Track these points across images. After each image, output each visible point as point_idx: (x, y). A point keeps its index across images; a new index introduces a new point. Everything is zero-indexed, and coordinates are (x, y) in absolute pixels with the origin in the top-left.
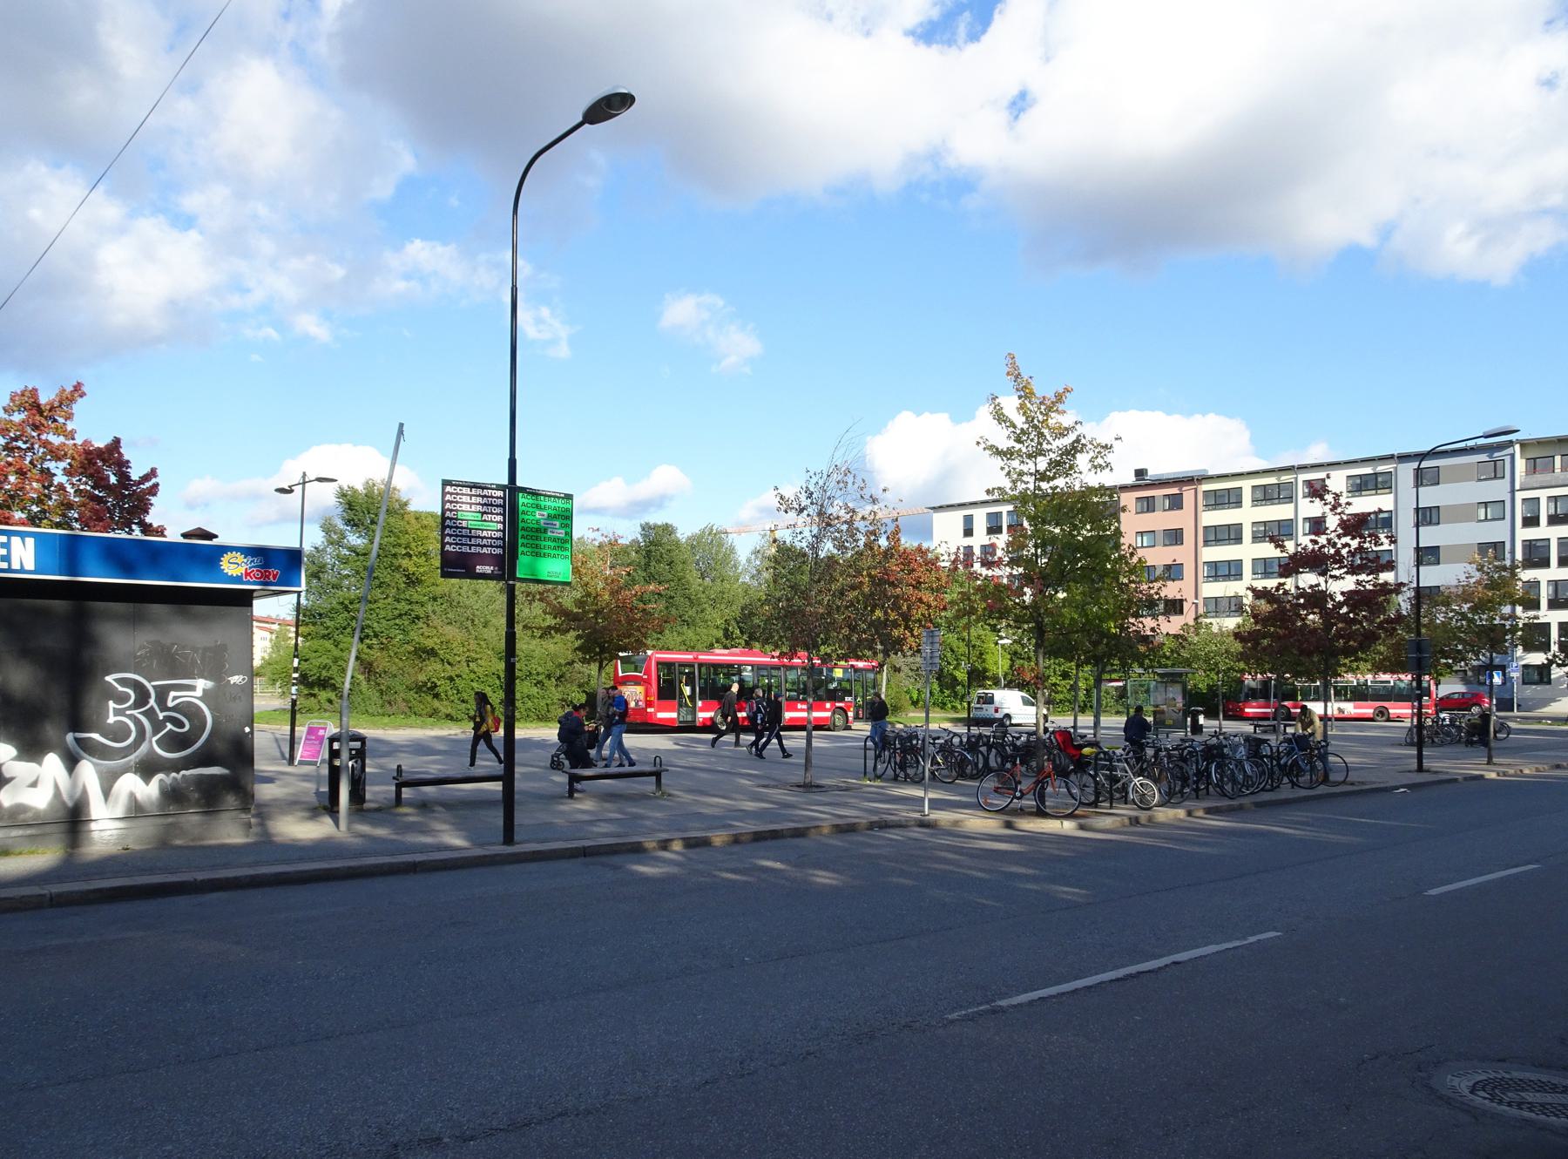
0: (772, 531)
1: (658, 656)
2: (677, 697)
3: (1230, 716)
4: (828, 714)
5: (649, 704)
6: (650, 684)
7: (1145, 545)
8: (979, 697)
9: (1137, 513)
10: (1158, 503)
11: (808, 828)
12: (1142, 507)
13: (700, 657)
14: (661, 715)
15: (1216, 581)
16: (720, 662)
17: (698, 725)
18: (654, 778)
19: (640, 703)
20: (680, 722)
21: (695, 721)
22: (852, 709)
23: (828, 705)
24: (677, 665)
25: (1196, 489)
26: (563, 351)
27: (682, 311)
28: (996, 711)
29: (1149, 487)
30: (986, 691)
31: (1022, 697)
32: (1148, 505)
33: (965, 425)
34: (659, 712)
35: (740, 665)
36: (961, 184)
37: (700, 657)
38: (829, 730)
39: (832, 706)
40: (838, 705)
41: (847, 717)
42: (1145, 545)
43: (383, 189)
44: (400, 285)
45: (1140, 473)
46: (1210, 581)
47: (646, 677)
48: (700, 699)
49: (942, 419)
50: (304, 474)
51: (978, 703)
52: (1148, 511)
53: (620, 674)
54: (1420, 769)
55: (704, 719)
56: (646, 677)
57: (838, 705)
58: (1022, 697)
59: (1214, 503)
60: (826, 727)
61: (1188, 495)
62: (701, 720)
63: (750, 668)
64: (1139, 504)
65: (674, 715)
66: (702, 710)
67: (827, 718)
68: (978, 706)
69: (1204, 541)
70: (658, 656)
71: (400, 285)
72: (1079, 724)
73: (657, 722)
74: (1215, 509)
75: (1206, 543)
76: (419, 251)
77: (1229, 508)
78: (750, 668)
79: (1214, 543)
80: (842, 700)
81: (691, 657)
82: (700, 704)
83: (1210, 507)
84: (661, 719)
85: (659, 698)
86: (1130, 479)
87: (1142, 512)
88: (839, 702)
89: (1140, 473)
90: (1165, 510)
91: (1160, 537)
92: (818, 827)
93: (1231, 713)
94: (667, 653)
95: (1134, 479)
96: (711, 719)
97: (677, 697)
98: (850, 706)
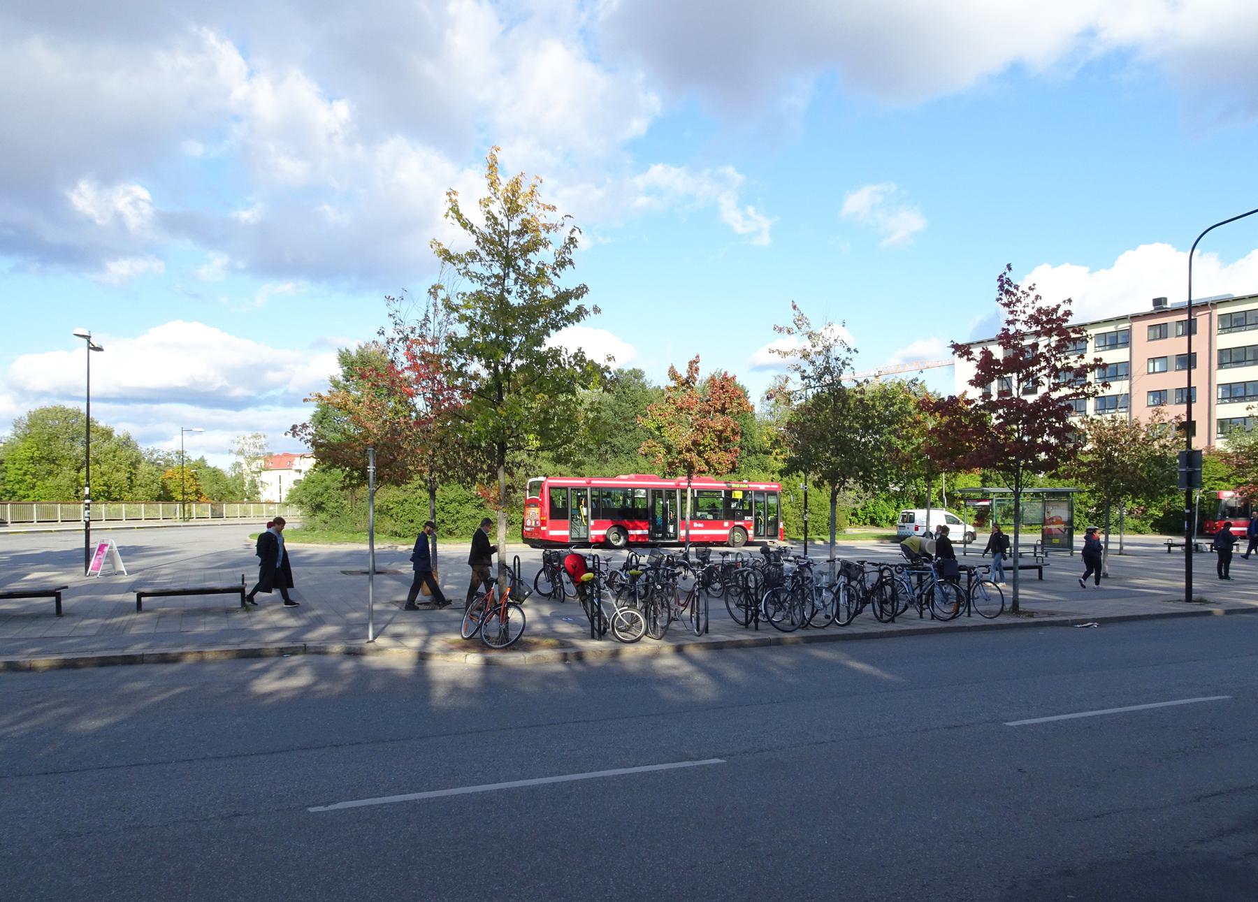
0: (876, 377)
1: (550, 481)
2: (570, 516)
3: (1207, 534)
4: (726, 532)
5: (543, 523)
6: (543, 506)
7: (1157, 370)
8: (904, 516)
9: (1149, 340)
10: (1171, 330)
11: (182, 654)
12: (1155, 335)
13: (593, 482)
14: (552, 533)
15: (1230, 402)
16: (599, 486)
17: (590, 541)
18: (1037, 570)
19: (537, 522)
20: (573, 539)
21: (587, 538)
22: (752, 527)
23: (726, 524)
24: (569, 489)
25: (1210, 314)
26: (765, 240)
27: (858, 201)
28: (917, 529)
29: (1176, 312)
30: (909, 511)
31: (946, 516)
32: (1161, 332)
33: (1103, 273)
34: (551, 530)
35: (633, 489)
36: (1122, 57)
37: (593, 482)
38: (728, 545)
39: (730, 525)
40: (736, 523)
41: (747, 534)
42: (1157, 370)
43: (638, 126)
44: (642, 201)
45: (1158, 302)
46: (1226, 403)
47: (540, 500)
48: (592, 519)
49: (1083, 270)
50: (99, 349)
51: (903, 521)
52: (1160, 338)
53: (528, 498)
54: (1189, 598)
55: (597, 536)
56: (540, 500)
57: (736, 523)
58: (946, 516)
59: (1229, 326)
60: (726, 543)
61: (1202, 319)
62: (593, 537)
63: (644, 491)
64: (1152, 332)
65: (566, 533)
66: (594, 528)
67: (725, 536)
68: (902, 524)
69: (1219, 364)
70: (550, 481)
71: (642, 201)
72: (1020, 542)
73: (550, 539)
74: (1231, 332)
75: (1221, 365)
76: (657, 172)
77: (1245, 330)
78: (644, 491)
79: (1252, 362)
80: (742, 519)
81: (584, 482)
82: (592, 523)
83: (1226, 331)
84: (552, 536)
85: (551, 518)
86: (1149, 308)
87: (1154, 340)
88: (738, 521)
89: (1158, 302)
90: (1177, 336)
91: (1173, 362)
92: (202, 652)
93: (1208, 532)
94: (604, 480)
95: (1152, 308)
96: (604, 536)
97: (570, 516)
98: (751, 525)
